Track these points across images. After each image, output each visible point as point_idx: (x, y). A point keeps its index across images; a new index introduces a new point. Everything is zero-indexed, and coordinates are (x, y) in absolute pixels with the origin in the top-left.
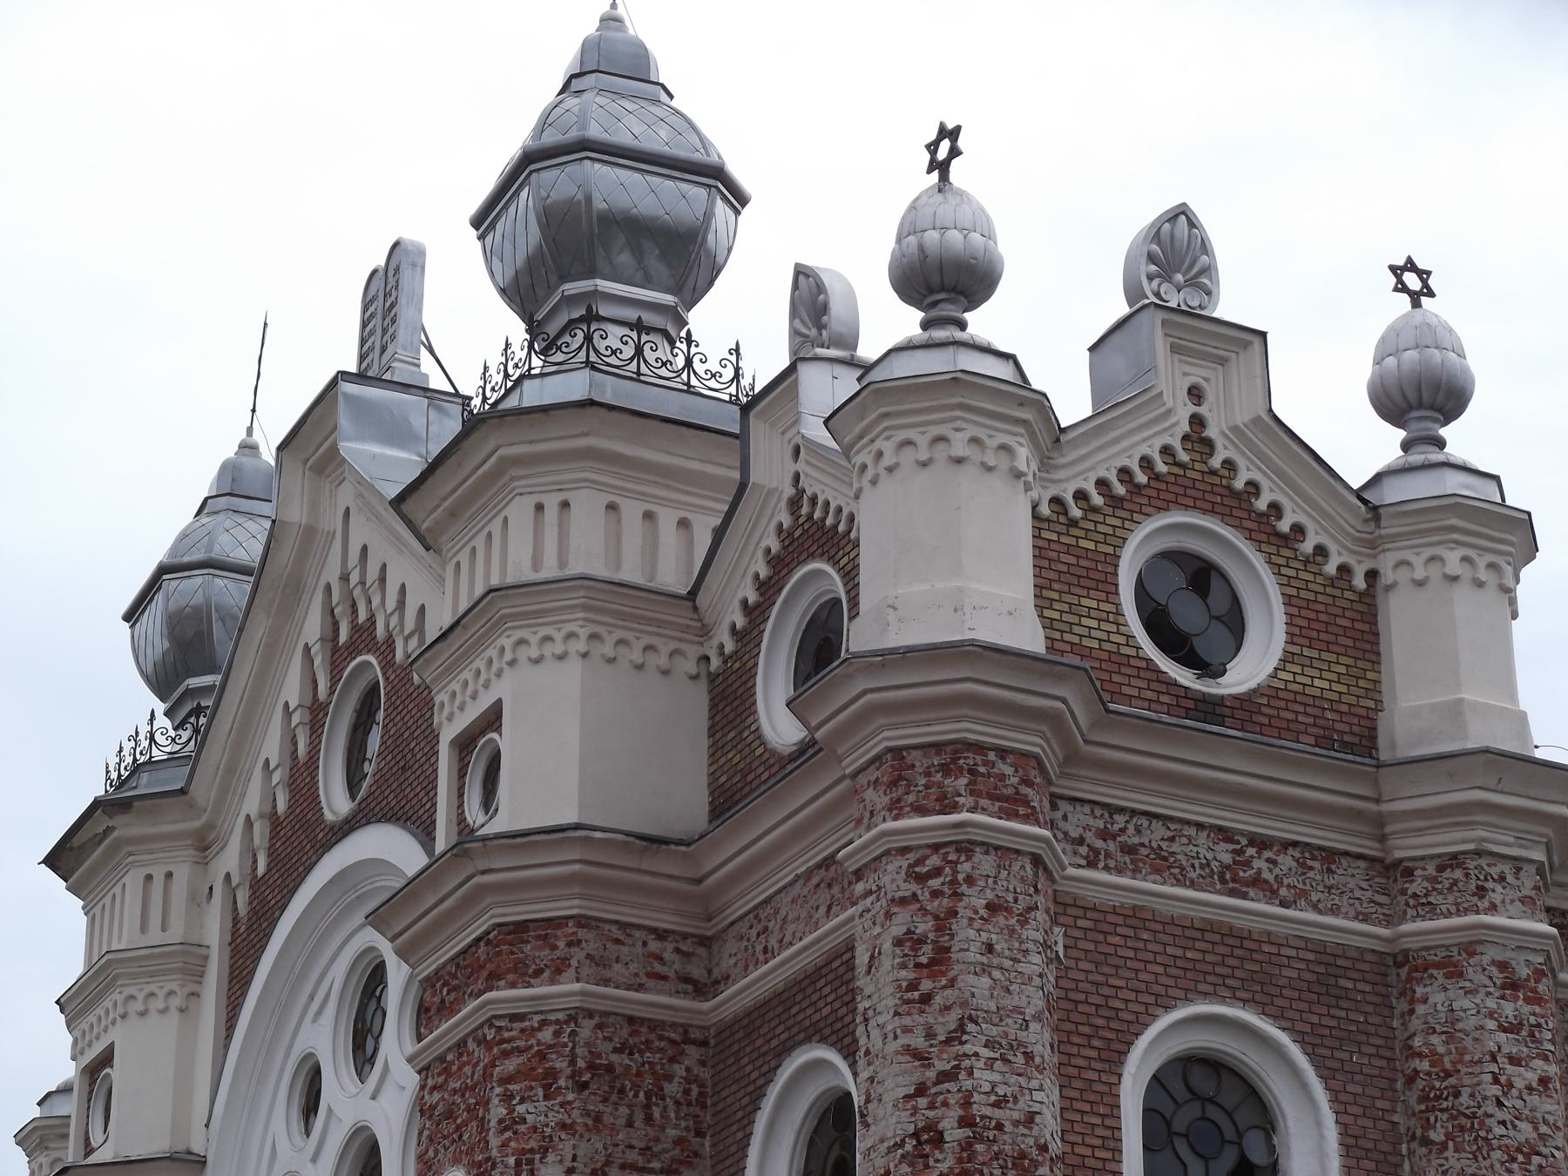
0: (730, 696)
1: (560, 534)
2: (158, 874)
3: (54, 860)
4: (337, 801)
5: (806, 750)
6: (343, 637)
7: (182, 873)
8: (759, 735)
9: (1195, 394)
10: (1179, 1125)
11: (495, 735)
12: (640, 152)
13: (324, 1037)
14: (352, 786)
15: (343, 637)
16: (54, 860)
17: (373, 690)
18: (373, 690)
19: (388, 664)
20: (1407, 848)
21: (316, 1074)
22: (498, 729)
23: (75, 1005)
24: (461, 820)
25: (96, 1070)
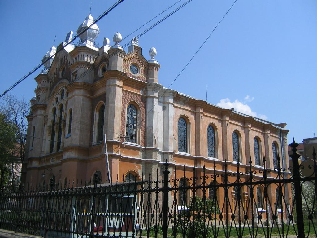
0: (96, 73)
1: (311, 140)
2: (44, 81)
3: (35, 79)
4: (61, 77)
5: (102, 77)
6: (62, 63)
7: (46, 81)
8: (98, 75)
9: (136, 52)
10: (130, 109)
11: (76, 73)
12: (227, 148)
13: (59, 96)
14: (62, 75)
15: (62, 63)
16: (35, 79)
17: (64, 68)
18: (64, 68)
19: (66, 66)
20: (9, 234)
21: (58, 98)
22: (77, 73)
23: (36, 91)
24: (73, 79)
25: (38, 97)
